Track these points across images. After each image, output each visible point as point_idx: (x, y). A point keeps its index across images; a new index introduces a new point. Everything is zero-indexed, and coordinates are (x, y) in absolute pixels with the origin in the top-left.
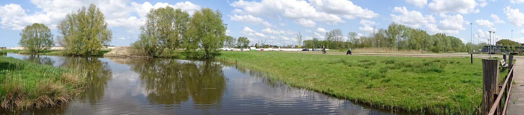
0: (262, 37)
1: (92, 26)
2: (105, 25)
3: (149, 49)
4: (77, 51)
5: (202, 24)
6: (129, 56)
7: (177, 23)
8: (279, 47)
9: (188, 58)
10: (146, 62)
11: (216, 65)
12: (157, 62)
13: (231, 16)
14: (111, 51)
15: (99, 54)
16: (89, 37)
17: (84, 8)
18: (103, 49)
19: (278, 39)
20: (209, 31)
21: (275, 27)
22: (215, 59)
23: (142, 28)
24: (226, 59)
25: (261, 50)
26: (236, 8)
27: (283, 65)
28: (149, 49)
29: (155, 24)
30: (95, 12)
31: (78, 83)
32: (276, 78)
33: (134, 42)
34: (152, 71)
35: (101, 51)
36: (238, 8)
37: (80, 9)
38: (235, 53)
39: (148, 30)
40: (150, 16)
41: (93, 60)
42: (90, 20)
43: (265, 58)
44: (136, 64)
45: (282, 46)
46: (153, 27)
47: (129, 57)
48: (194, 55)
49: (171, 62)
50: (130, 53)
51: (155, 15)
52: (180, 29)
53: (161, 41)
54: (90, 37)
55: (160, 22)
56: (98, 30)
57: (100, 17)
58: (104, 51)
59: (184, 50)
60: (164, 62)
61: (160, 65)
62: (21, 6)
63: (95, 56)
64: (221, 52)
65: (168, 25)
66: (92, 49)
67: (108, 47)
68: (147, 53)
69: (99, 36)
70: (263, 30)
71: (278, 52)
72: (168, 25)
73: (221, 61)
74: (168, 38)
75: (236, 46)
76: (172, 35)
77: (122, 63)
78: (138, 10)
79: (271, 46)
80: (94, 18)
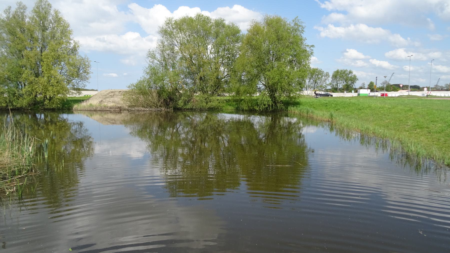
0: (384, 69)
1: (43, 48)
2: (75, 46)
3: (165, 94)
4: (8, 101)
5: (265, 46)
6: (127, 108)
7: (217, 46)
8: (425, 89)
9: (238, 111)
10: (161, 119)
11: (290, 123)
12: (182, 118)
13: (321, 29)
14: (88, 99)
15: (63, 106)
16: (38, 70)
17: (22, 7)
18: (71, 96)
19: (421, 71)
20: (278, 59)
21: (417, 44)
22: (289, 111)
23: (152, 55)
24: (310, 111)
25: (383, 95)
26: (332, 11)
27: (440, 127)
28: (165, 94)
29: (176, 48)
30: (50, 18)
31: (10, 168)
32: (423, 152)
33: (135, 82)
34: (171, 136)
35: (68, 101)
36: (338, 12)
37: (10, 7)
38: (327, 102)
39: (162, 59)
40: (165, 32)
41: (48, 119)
42: (38, 34)
43: (393, 111)
44: (142, 124)
45: (433, 87)
46: (173, 52)
47: (128, 110)
48: (250, 105)
49: (207, 117)
50: (129, 103)
51: (175, 30)
52: (222, 57)
53: (188, 80)
54: (40, 70)
55: (186, 44)
56: (59, 55)
57: (61, 28)
58: (73, 99)
59: (230, 96)
60: (194, 118)
61: (187, 124)
63: (53, 110)
64: (300, 99)
65: (201, 49)
66: (45, 97)
67: (82, 92)
68: (162, 103)
69: (62, 69)
70: (389, 54)
71: (422, 100)
72: (201, 49)
73: (301, 117)
74: (201, 74)
75: (329, 87)
76: (207, 67)
77: (114, 122)
78: (142, 20)
79: (405, 87)
80: (47, 30)
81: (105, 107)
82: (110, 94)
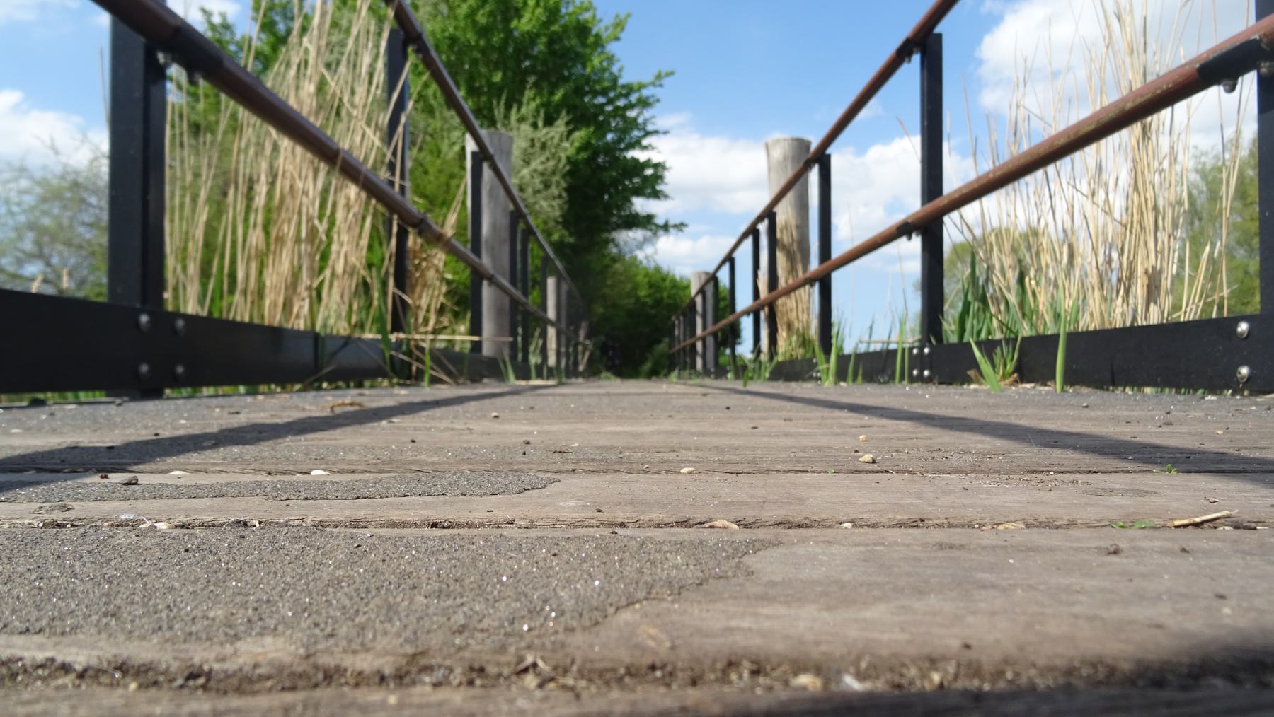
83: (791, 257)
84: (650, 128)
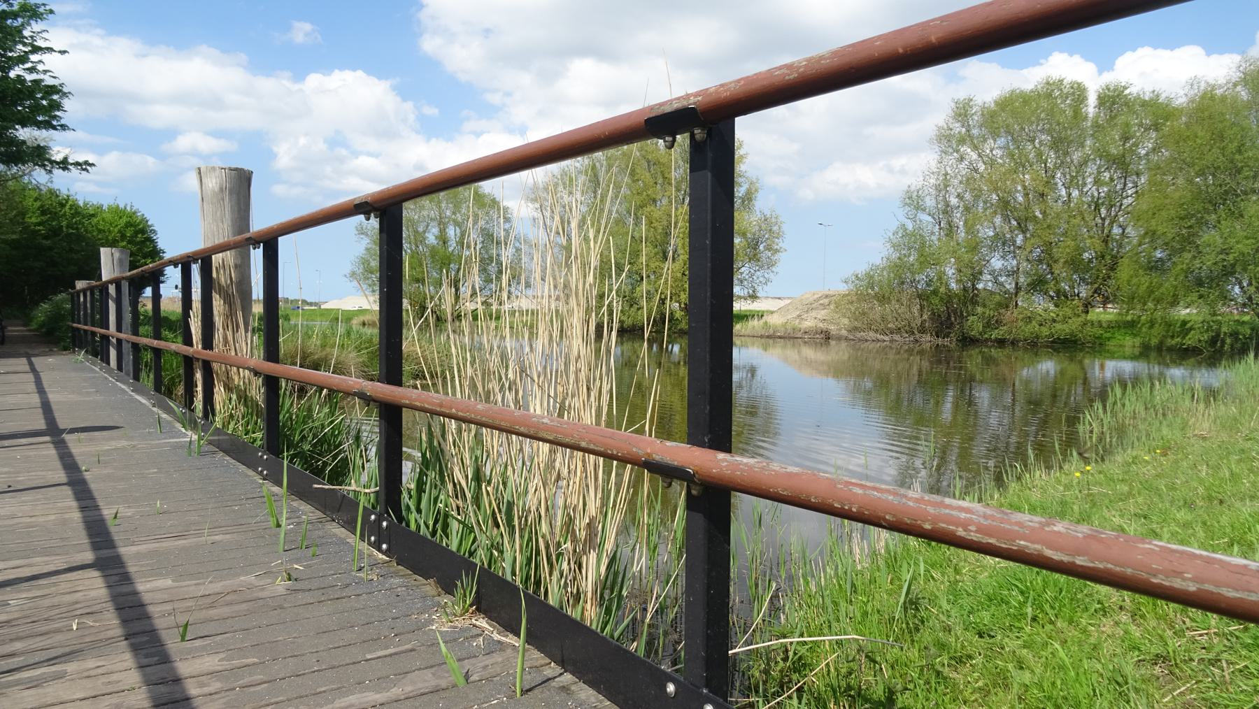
6: (844, 333)
23: (913, 201)
47: (846, 339)
62: (394, 88)
81: (794, 329)
82: (821, 302)
83: (228, 300)
84: (40, 43)
